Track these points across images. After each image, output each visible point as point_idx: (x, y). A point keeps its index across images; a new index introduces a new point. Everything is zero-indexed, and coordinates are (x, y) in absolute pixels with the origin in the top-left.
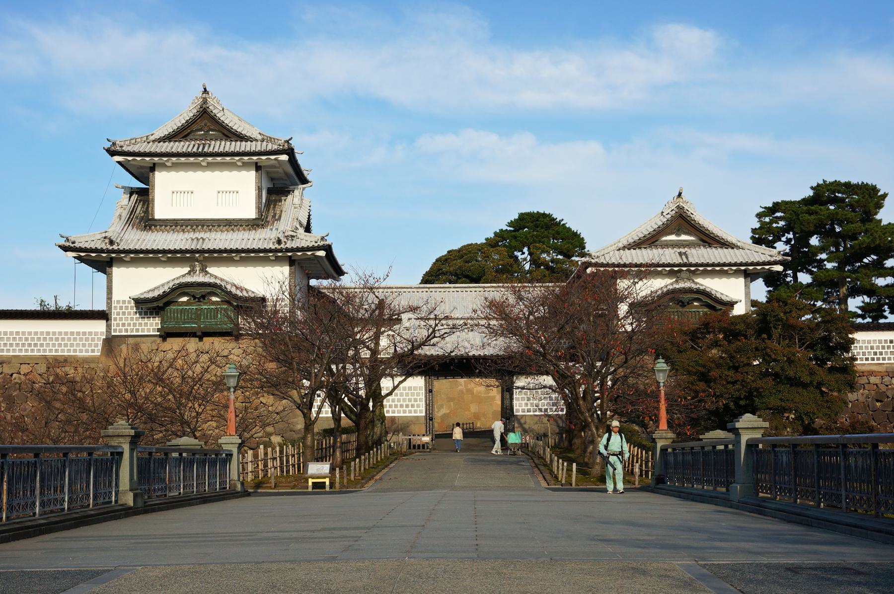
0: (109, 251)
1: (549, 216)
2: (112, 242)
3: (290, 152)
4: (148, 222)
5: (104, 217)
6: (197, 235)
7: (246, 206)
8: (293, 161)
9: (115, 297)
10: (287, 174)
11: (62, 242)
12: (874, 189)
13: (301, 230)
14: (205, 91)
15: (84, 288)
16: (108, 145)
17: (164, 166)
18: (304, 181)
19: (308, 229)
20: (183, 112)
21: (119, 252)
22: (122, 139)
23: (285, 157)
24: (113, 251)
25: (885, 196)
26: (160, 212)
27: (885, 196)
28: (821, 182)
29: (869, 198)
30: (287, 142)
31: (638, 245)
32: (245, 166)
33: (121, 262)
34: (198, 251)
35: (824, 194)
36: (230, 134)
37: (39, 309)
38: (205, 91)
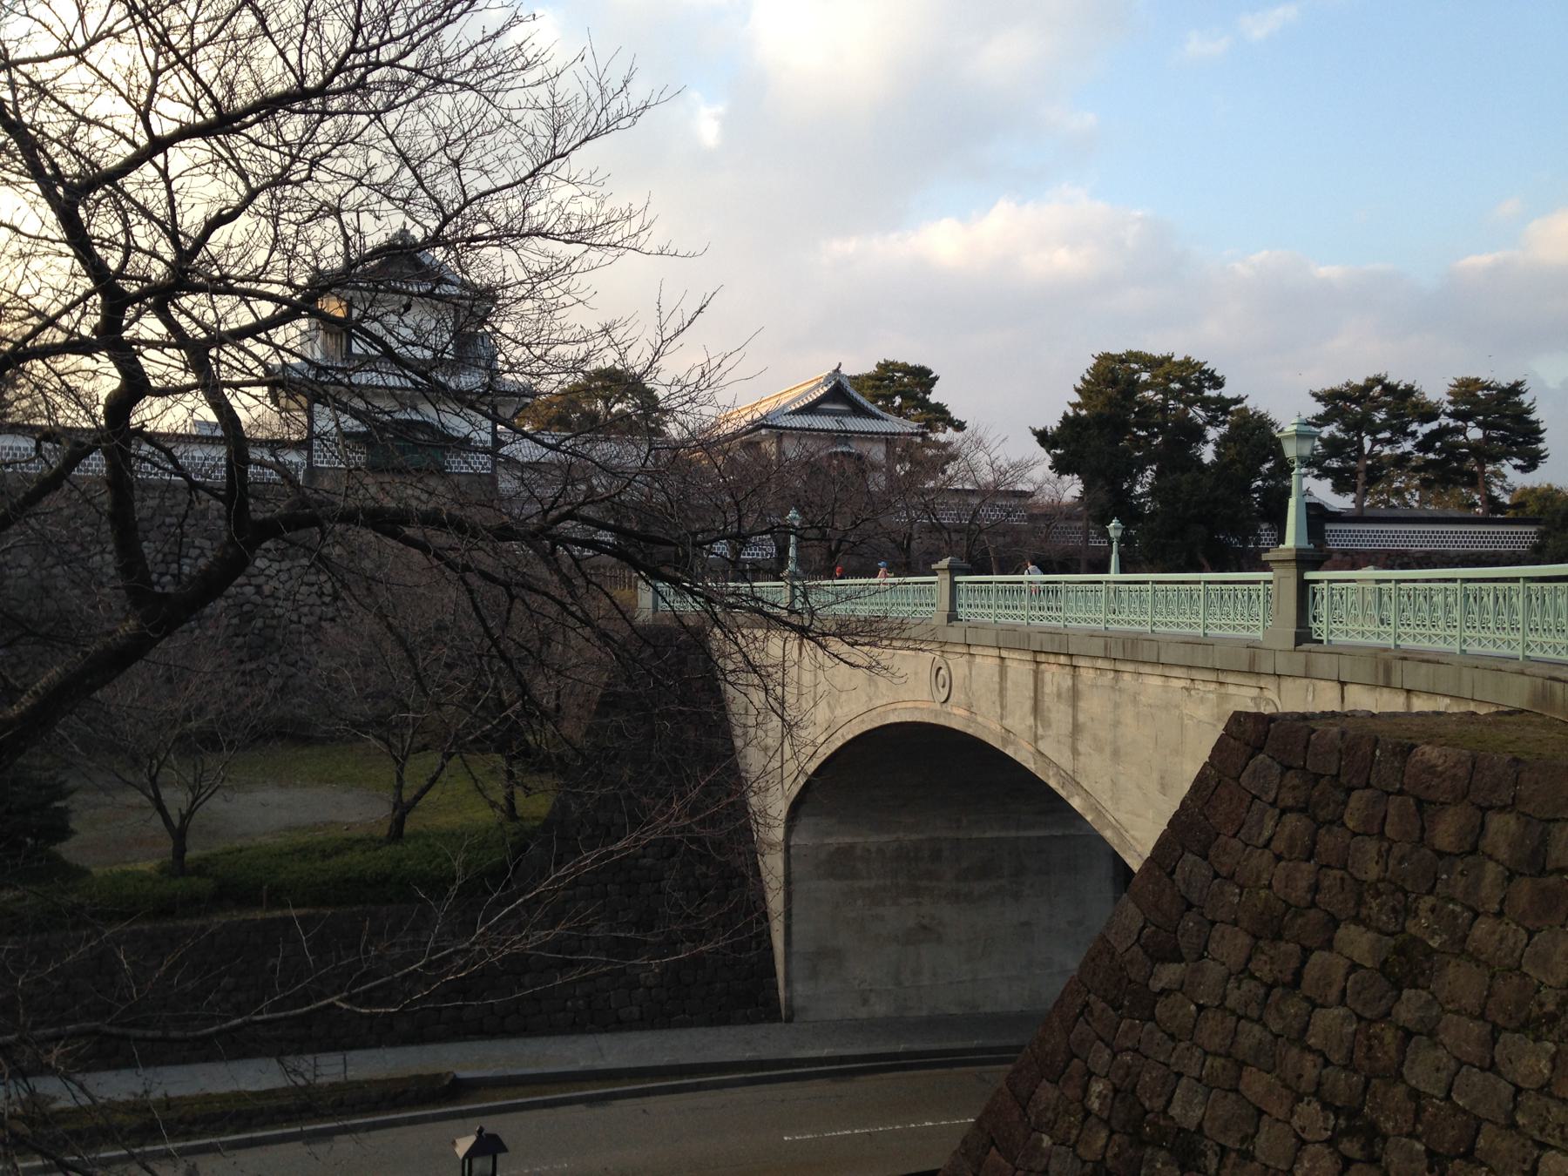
12: (930, 372)
25: (936, 378)
27: (936, 378)
29: (924, 378)
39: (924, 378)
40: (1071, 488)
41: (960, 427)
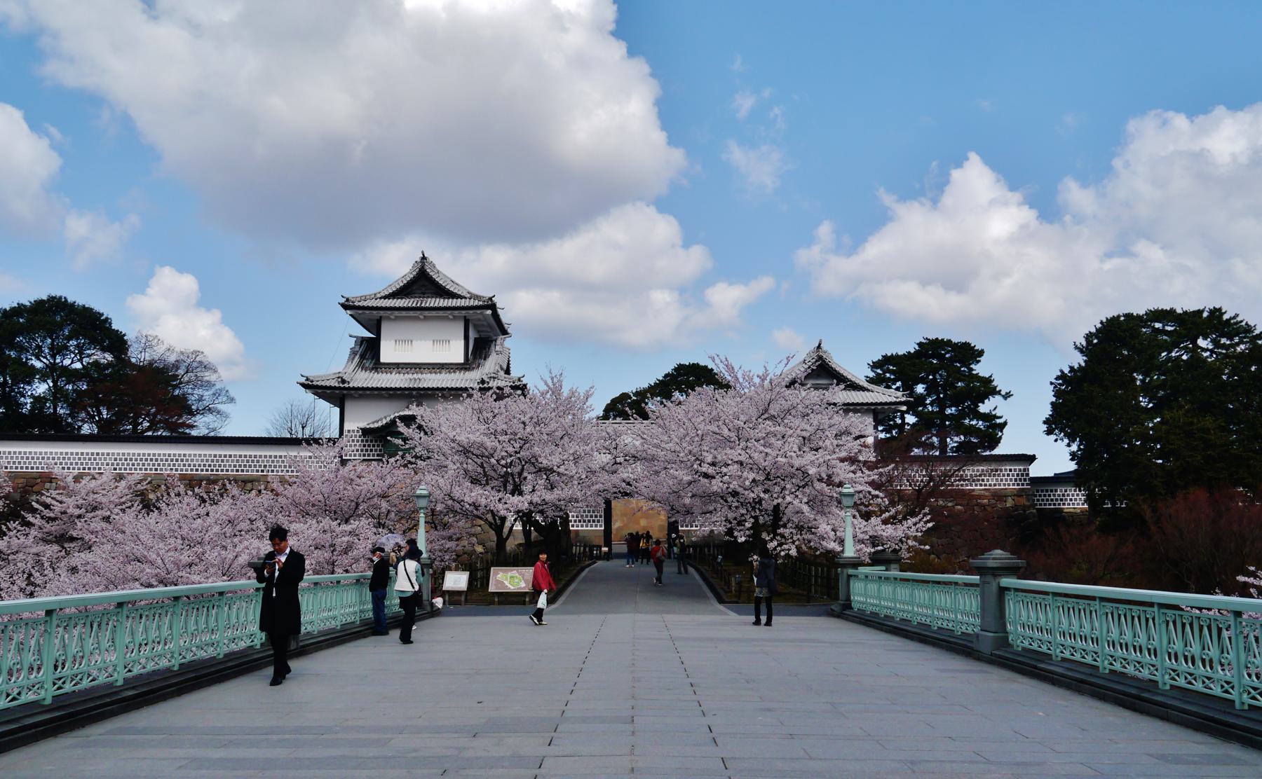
0: (339, 388)
1: (1213, 322)
2: (343, 381)
3: (493, 307)
4: (378, 366)
5: (334, 357)
6: (415, 376)
7: (454, 351)
8: (496, 316)
9: (346, 427)
10: (490, 326)
11: (303, 380)
13: (502, 373)
14: (424, 258)
15: (326, 415)
16: (343, 300)
17: (388, 318)
18: (505, 332)
19: (508, 372)
21: (349, 389)
22: (355, 292)
23: (489, 312)
24: (344, 388)
26: (385, 357)
28: (1099, 326)
30: (490, 299)
31: (385, 297)
32: (455, 318)
33: (352, 397)
34: (414, 389)
35: (931, 348)
36: (443, 292)
37: (1171, 114)
38: (424, 258)
39: (969, 353)
40: (1055, 457)
41: (232, 400)
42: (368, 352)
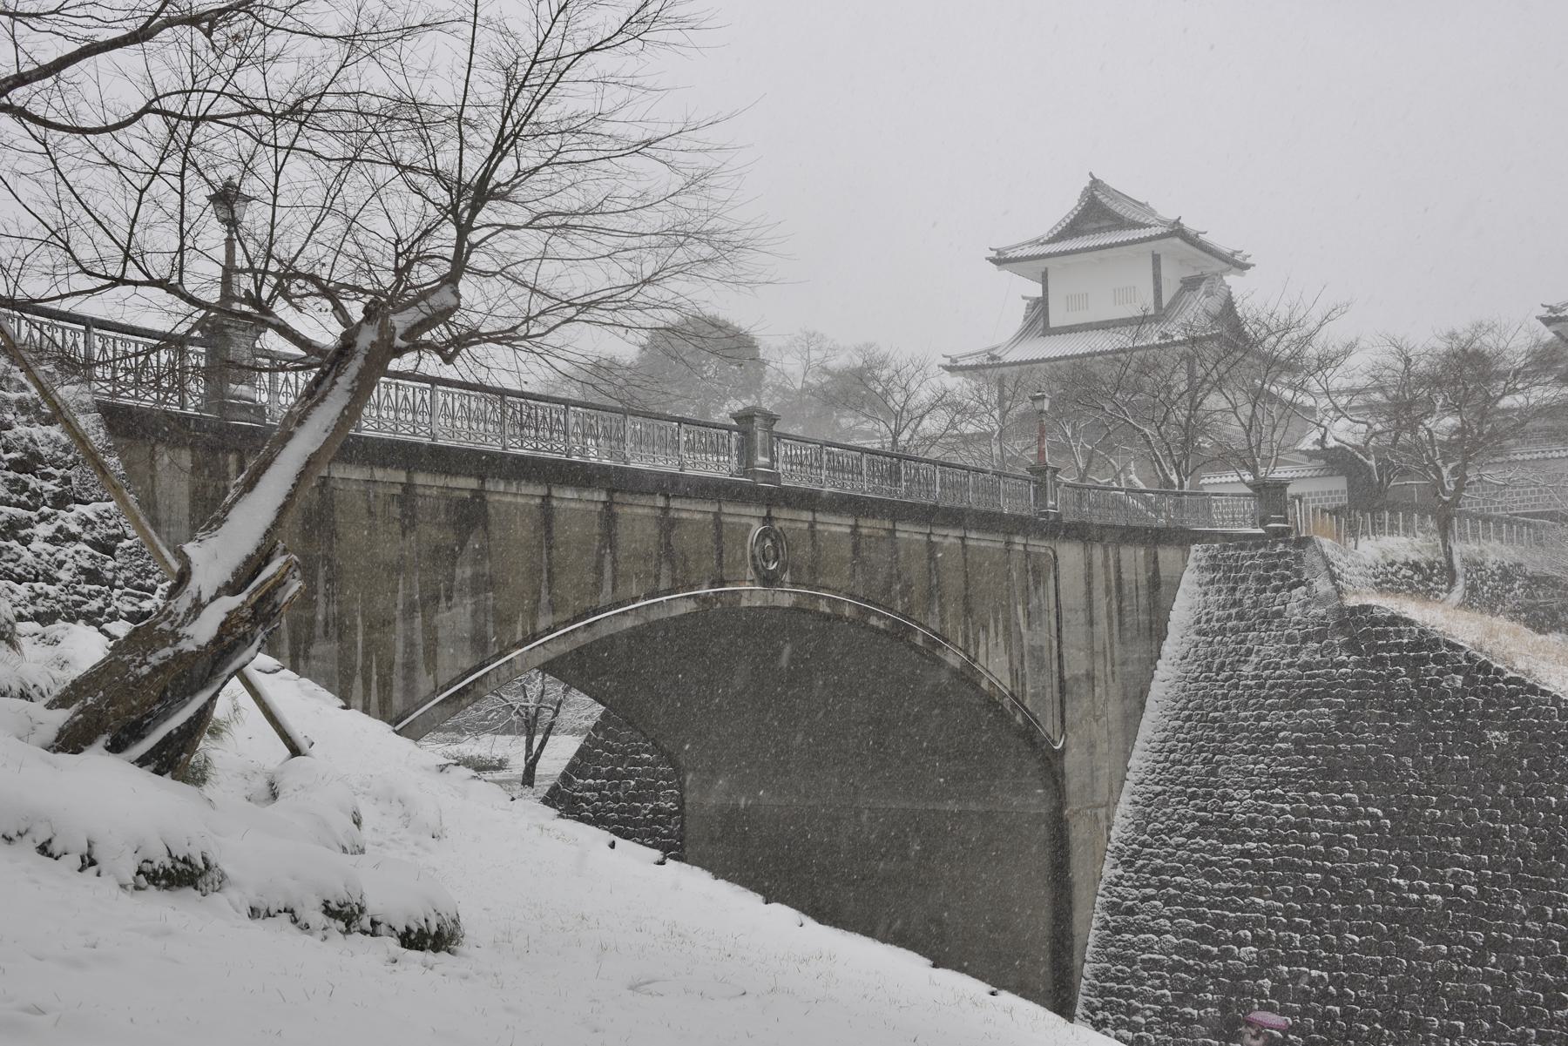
2: (993, 358)
4: (1048, 331)
20: (1067, 204)
30: (1177, 222)
36: (1120, 223)
38: (1095, 183)
42: (1038, 318)
